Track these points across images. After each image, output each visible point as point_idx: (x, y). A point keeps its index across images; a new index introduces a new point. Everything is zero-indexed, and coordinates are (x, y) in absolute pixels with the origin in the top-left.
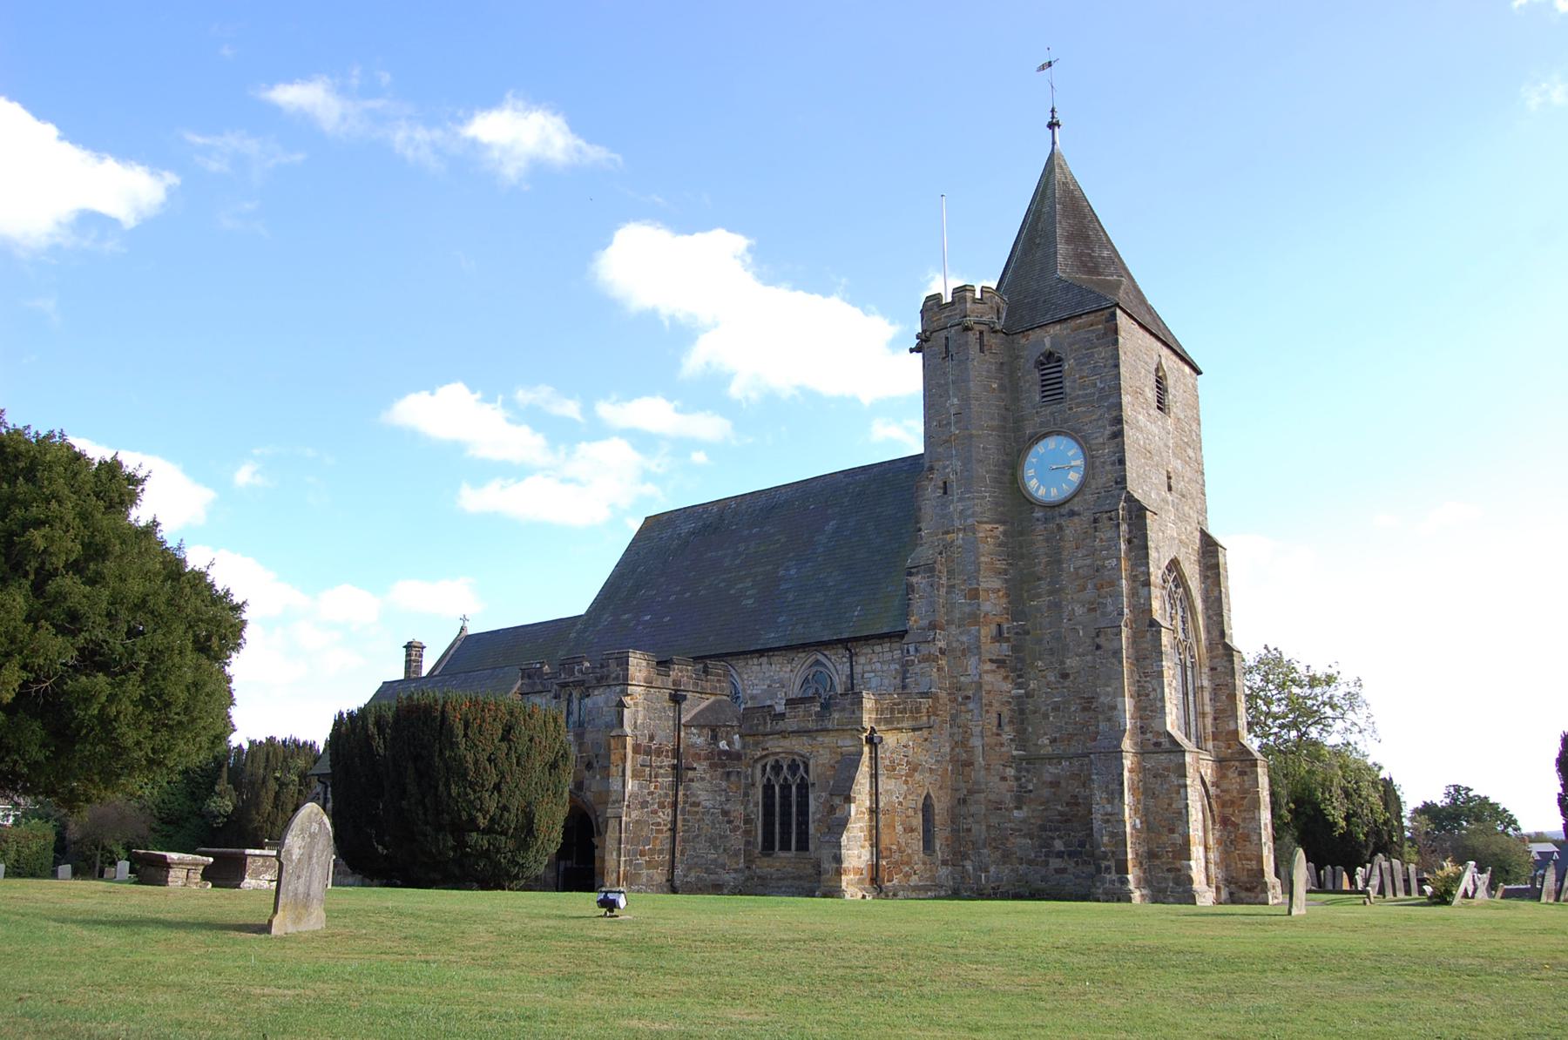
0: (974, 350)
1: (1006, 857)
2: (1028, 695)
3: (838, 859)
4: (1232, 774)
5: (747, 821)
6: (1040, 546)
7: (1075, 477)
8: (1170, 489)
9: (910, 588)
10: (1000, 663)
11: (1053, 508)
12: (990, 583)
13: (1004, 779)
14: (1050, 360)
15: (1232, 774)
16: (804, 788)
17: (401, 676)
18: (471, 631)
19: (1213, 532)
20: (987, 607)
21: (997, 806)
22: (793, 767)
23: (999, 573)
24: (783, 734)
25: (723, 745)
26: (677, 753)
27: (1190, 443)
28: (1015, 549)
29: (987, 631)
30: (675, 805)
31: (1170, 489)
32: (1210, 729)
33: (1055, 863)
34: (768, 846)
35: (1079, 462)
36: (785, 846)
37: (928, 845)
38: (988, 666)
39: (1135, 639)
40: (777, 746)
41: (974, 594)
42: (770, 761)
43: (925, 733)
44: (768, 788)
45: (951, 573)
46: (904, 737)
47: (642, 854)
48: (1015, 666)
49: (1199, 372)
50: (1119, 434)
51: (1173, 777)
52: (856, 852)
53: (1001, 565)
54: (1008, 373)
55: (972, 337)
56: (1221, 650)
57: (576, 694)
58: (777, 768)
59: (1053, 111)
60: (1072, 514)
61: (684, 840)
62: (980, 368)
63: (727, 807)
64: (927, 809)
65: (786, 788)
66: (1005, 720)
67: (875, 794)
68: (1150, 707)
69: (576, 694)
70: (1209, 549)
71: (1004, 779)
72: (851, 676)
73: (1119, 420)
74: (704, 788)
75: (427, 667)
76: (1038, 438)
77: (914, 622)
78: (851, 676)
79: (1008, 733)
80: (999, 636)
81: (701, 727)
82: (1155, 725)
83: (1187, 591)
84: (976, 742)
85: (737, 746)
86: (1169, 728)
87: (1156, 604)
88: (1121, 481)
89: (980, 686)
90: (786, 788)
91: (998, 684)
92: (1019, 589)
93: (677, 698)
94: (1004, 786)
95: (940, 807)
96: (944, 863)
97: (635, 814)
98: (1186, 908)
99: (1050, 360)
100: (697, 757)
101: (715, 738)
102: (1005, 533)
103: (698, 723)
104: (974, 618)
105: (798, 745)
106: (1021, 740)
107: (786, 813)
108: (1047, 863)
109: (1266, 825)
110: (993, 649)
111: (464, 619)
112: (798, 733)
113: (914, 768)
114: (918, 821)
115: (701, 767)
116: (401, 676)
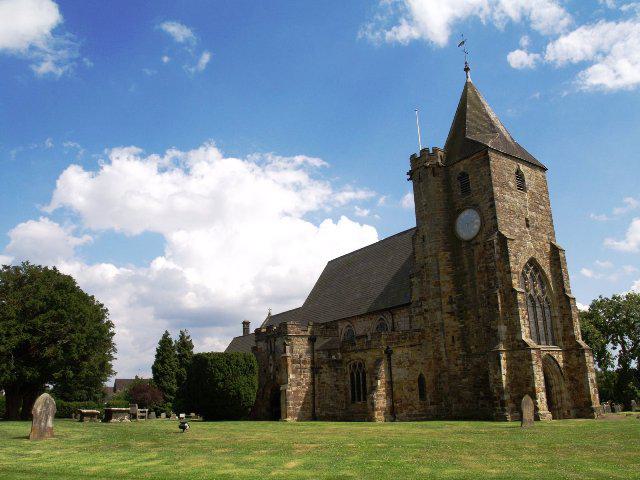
0: (430, 176)
1: (460, 400)
2: (465, 327)
3: (373, 404)
4: (573, 357)
5: (346, 389)
6: (466, 261)
7: (477, 227)
9: (411, 284)
10: (452, 313)
11: (469, 242)
12: (445, 278)
13: (457, 365)
14: (463, 176)
15: (573, 357)
16: (364, 373)
17: (242, 334)
18: (273, 314)
19: (559, 243)
20: (444, 289)
21: (455, 377)
22: (360, 365)
23: (448, 274)
25: (333, 357)
27: (541, 201)
28: (455, 262)
29: (445, 300)
32: (561, 336)
33: (481, 402)
34: (353, 400)
35: (478, 221)
37: (422, 395)
38: (446, 315)
39: (504, 299)
40: (353, 356)
41: (438, 284)
43: (418, 347)
44: (352, 374)
45: (428, 275)
46: (406, 350)
48: (459, 314)
49: (544, 169)
50: (493, 206)
51: (526, 361)
52: (381, 401)
53: (450, 270)
54: (447, 182)
55: (429, 171)
56: (564, 298)
57: (273, 340)
58: (355, 366)
59: (467, 70)
60: (477, 244)
61: (319, 398)
62: (434, 184)
63: (337, 383)
64: (421, 380)
65: (358, 375)
66: (456, 339)
67: (390, 374)
68: (515, 329)
69: (273, 340)
70: (555, 254)
71: (457, 365)
72: (393, 323)
73: (492, 199)
74: (326, 376)
76: (460, 211)
77: (415, 297)
78: (393, 323)
79: (457, 344)
80: (451, 302)
81: (323, 350)
82: (518, 337)
83: (543, 272)
84: (443, 349)
85: (340, 357)
87: (514, 281)
88: (496, 227)
89: (443, 324)
90: (358, 375)
91: (453, 324)
92: (458, 280)
94: (457, 369)
95: (429, 379)
96: (432, 404)
97: (294, 389)
98: (334, 432)
99: (463, 176)
100: (323, 363)
101: (330, 356)
102: (451, 255)
104: (439, 294)
105: (360, 355)
106: (465, 347)
107: (358, 385)
108: (477, 403)
109: (592, 380)
110: (447, 308)
112: (361, 350)
113: (412, 363)
114: (416, 386)
115: (325, 367)
116: (242, 334)
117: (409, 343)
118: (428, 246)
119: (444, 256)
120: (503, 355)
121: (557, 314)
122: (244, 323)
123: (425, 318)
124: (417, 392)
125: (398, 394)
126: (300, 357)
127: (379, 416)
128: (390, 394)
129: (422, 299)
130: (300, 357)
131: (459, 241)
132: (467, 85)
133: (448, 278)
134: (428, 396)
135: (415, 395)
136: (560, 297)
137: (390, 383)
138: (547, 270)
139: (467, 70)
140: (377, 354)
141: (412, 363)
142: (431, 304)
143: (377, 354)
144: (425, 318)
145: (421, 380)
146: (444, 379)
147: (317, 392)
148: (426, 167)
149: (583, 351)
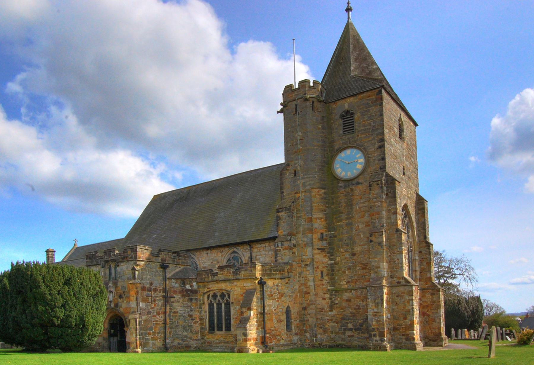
0: (310, 110)
8: (404, 174)
10: (322, 250)
11: (349, 182)
12: (318, 215)
13: (324, 299)
14: (348, 115)
15: (428, 295)
16: (228, 304)
18: (79, 245)
20: (316, 225)
24: (218, 281)
26: (165, 291)
29: (316, 236)
30: (165, 313)
31: (404, 174)
33: (348, 333)
34: (212, 329)
35: (362, 160)
36: (220, 329)
38: (317, 251)
40: (214, 287)
41: (310, 220)
42: (211, 293)
43: (287, 280)
44: (211, 305)
46: (277, 282)
47: (149, 334)
49: (416, 124)
56: (424, 244)
57: (113, 265)
59: (348, 10)
60: (358, 183)
61: (171, 328)
63: (191, 313)
64: (288, 312)
65: (219, 304)
66: (325, 274)
69: (113, 265)
70: (420, 203)
71: (324, 299)
75: (59, 258)
76: (341, 150)
79: (326, 279)
80: (322, 239)
84: (311, 284)
86: (405, 275)
89: (313, 260)
90: (219, 304)
91: (322, 259)
93: (164, 267)
94: (324, 302)
95: (294, 312)
96: (296, 334)
99: (348, 115)
100: (175, 292)
101: (184, 284)
103: (175, 277)
104: (311, 230)
105: (224, 286)
106: (332, 282)
110: (318, 244)
111: (76, 241)
112: (225, 281)
113: (282, 295)
114: (284, 317)
115: (178, 297)
117: (280, 276)
118: (300, 182)
119: (317, 194)
120: (385, 290)
121: (417, 258)
122: (48, 251)
123: (293, 253)
124: (284, 323)
125: (268, 326)
126: (151, 284)
127: (252, 347)
128: (262, 325)
129: (290, 234)
130: (151, 284)
131: (336, 179)
132: (348, 28)
133: (321, 215)
134: (293, 327)
135: (283, 326)
136: (420, 242)
137: (262, 314)
138: (413, 216)
139: (348, 10)
140: (248, 285)
141: (282, 295)
142: (301, 239)
143: (248, 285)
144: (293, 253)
145: (288, 312)
146: (310, 312)
147: (168, 320)
148: (306, 100)
149: (438, 290)
